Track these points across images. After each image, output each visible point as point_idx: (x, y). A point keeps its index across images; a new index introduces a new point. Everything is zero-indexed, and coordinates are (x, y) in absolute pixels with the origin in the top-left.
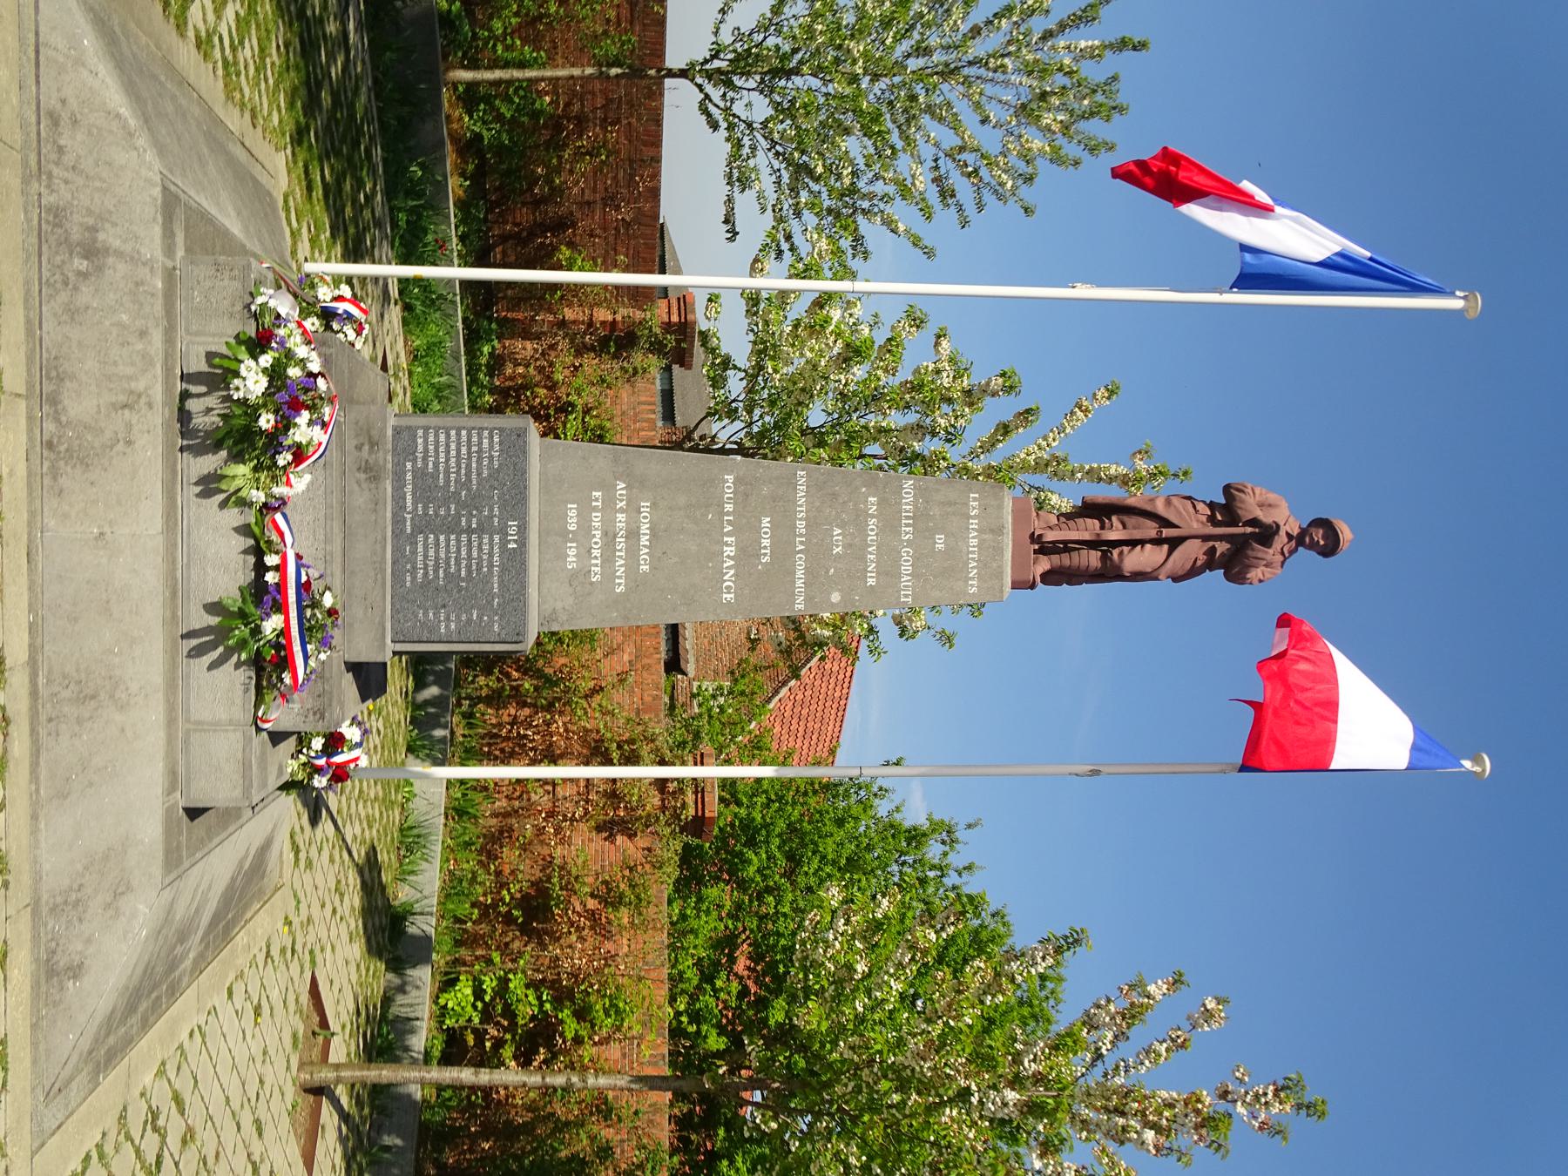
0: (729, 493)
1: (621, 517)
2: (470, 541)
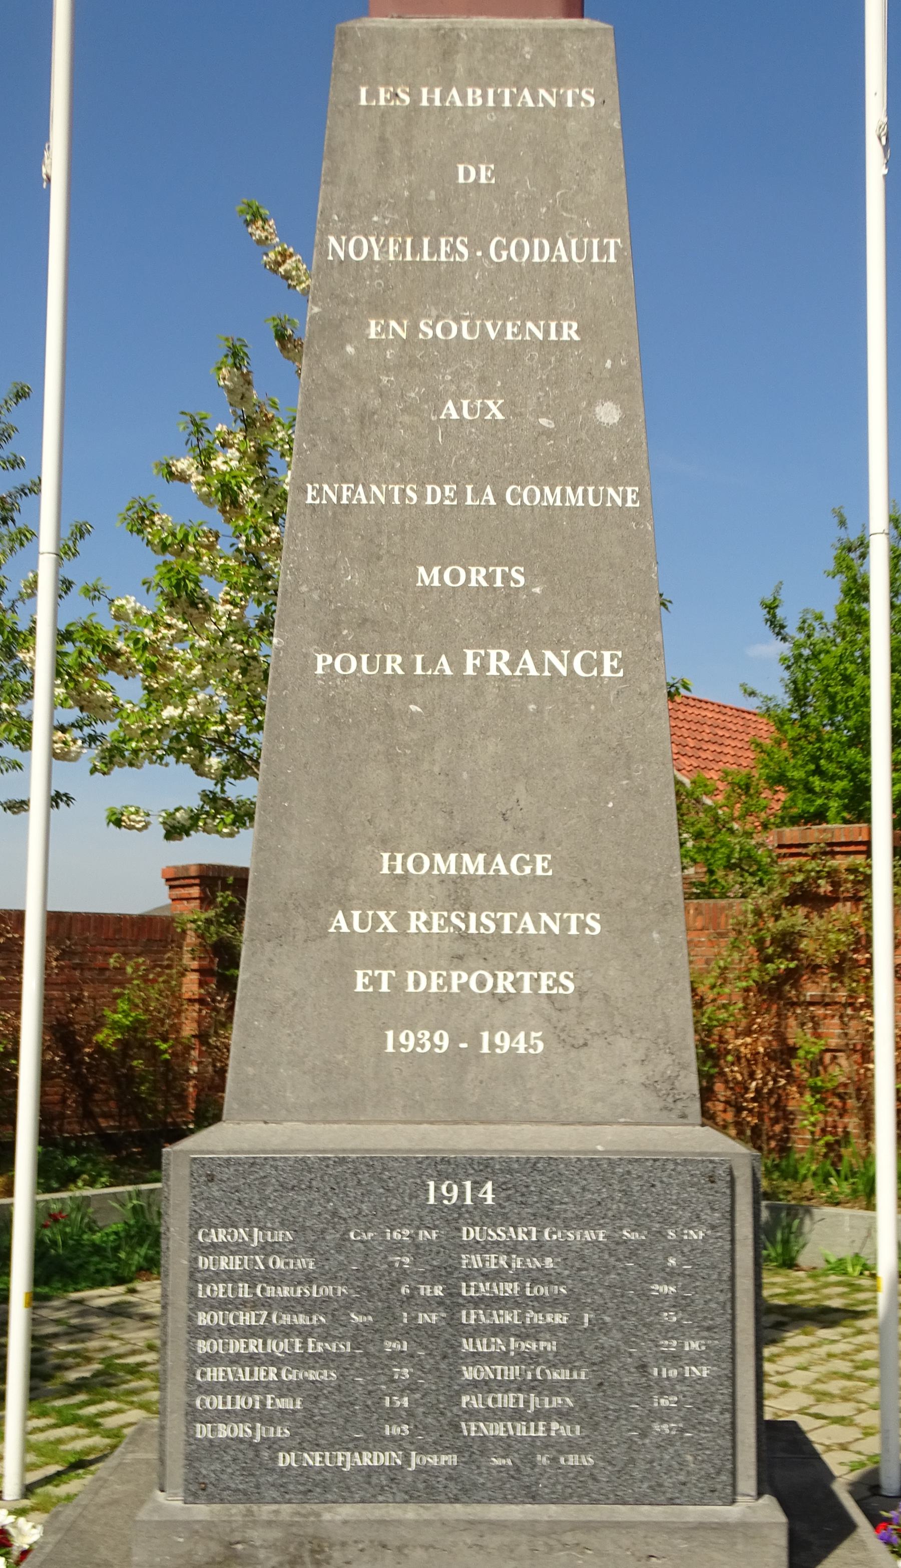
0: (359, 665)
2: (477, 1302)
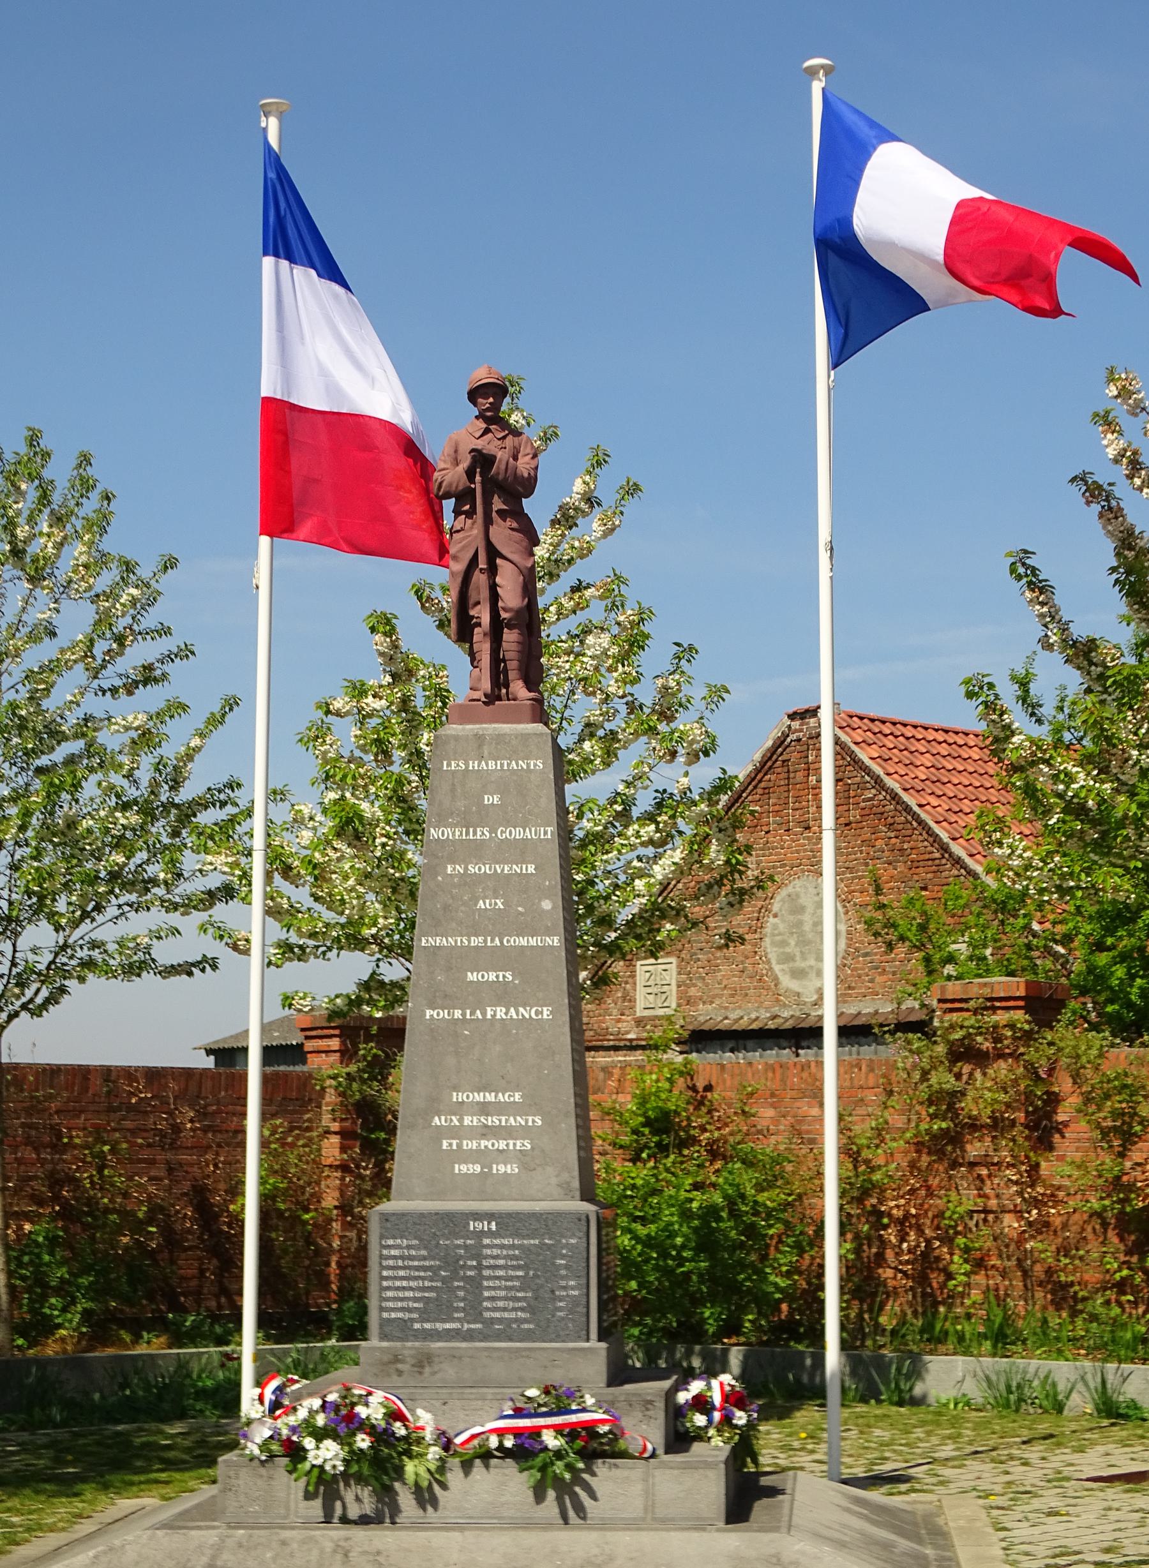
0: (444, 1014)
1: (467, 1121)
2: (488, 1267)
